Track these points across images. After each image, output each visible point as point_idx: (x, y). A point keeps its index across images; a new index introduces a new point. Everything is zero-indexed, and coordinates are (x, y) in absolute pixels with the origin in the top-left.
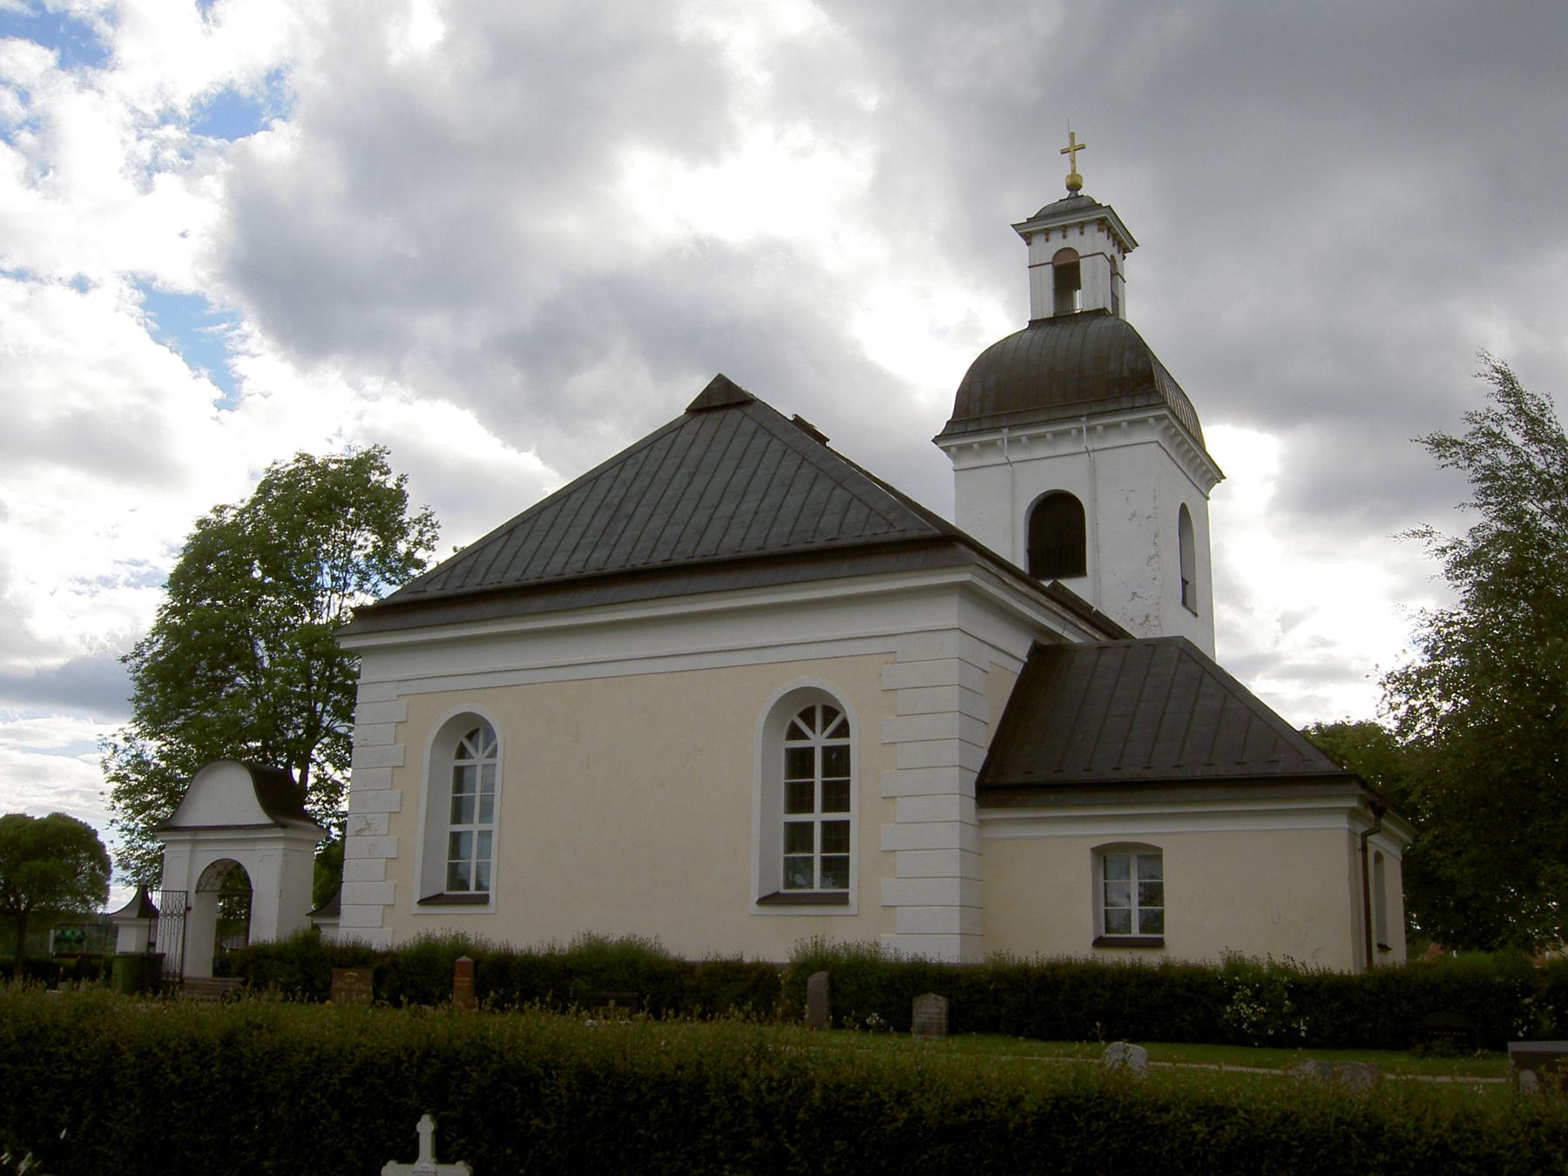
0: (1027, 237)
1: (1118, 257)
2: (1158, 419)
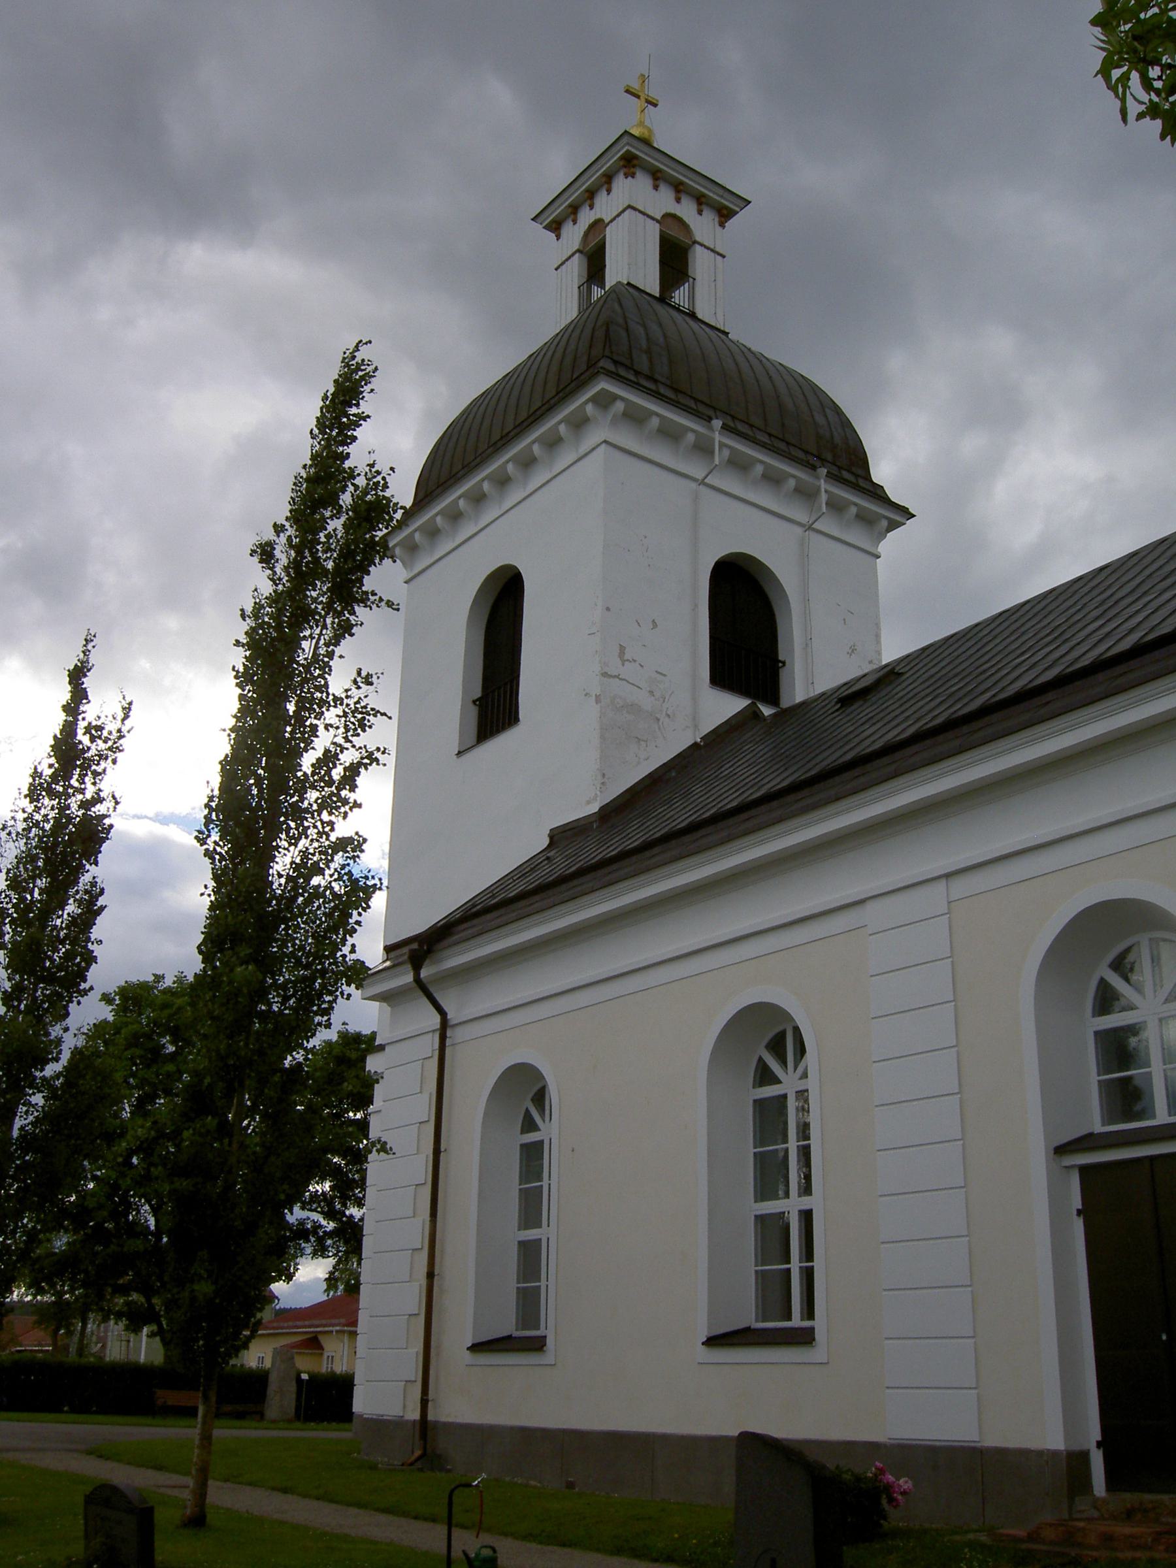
0: (555, 227)
1: (702, 226)
2: (604, 401)
